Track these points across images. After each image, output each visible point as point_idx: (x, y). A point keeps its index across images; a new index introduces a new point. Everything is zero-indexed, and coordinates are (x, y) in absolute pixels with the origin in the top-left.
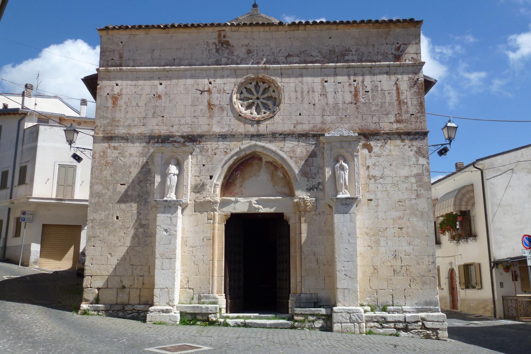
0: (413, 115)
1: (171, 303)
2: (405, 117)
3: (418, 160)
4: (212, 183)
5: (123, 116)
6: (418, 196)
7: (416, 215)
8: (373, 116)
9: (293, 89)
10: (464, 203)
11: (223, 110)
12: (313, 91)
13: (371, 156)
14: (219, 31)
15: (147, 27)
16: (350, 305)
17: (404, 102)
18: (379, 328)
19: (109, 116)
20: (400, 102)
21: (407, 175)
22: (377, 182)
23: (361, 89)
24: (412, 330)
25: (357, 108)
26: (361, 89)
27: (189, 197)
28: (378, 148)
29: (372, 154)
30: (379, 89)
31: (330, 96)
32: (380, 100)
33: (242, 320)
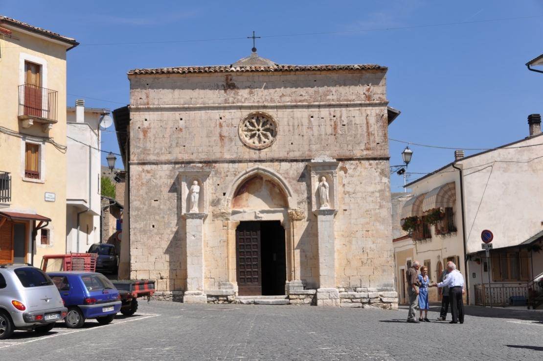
0: (379, 143)
1: (200, 289)
2: (373, 145)
3: (381, 179)
6: (381, 207)
9: (286, 123)
10: (445, 200)
11: (232, 141)
12: (302, 125)
13: (346, 176)
14: (227, 75)
16: (329, 287)
17: (372, 134)
18: (349, 303)
19: (141, 146)
21: (373, 191)
22: (351, 196)
23: (339, 123)
24: (373, 303)
25: (336, 138)
26: (339, 123)
28: (351, 170)
29: (347, 175)
30: (353, 123)
31: (315, 129)
32: (354, 132)
33: (253, 300)
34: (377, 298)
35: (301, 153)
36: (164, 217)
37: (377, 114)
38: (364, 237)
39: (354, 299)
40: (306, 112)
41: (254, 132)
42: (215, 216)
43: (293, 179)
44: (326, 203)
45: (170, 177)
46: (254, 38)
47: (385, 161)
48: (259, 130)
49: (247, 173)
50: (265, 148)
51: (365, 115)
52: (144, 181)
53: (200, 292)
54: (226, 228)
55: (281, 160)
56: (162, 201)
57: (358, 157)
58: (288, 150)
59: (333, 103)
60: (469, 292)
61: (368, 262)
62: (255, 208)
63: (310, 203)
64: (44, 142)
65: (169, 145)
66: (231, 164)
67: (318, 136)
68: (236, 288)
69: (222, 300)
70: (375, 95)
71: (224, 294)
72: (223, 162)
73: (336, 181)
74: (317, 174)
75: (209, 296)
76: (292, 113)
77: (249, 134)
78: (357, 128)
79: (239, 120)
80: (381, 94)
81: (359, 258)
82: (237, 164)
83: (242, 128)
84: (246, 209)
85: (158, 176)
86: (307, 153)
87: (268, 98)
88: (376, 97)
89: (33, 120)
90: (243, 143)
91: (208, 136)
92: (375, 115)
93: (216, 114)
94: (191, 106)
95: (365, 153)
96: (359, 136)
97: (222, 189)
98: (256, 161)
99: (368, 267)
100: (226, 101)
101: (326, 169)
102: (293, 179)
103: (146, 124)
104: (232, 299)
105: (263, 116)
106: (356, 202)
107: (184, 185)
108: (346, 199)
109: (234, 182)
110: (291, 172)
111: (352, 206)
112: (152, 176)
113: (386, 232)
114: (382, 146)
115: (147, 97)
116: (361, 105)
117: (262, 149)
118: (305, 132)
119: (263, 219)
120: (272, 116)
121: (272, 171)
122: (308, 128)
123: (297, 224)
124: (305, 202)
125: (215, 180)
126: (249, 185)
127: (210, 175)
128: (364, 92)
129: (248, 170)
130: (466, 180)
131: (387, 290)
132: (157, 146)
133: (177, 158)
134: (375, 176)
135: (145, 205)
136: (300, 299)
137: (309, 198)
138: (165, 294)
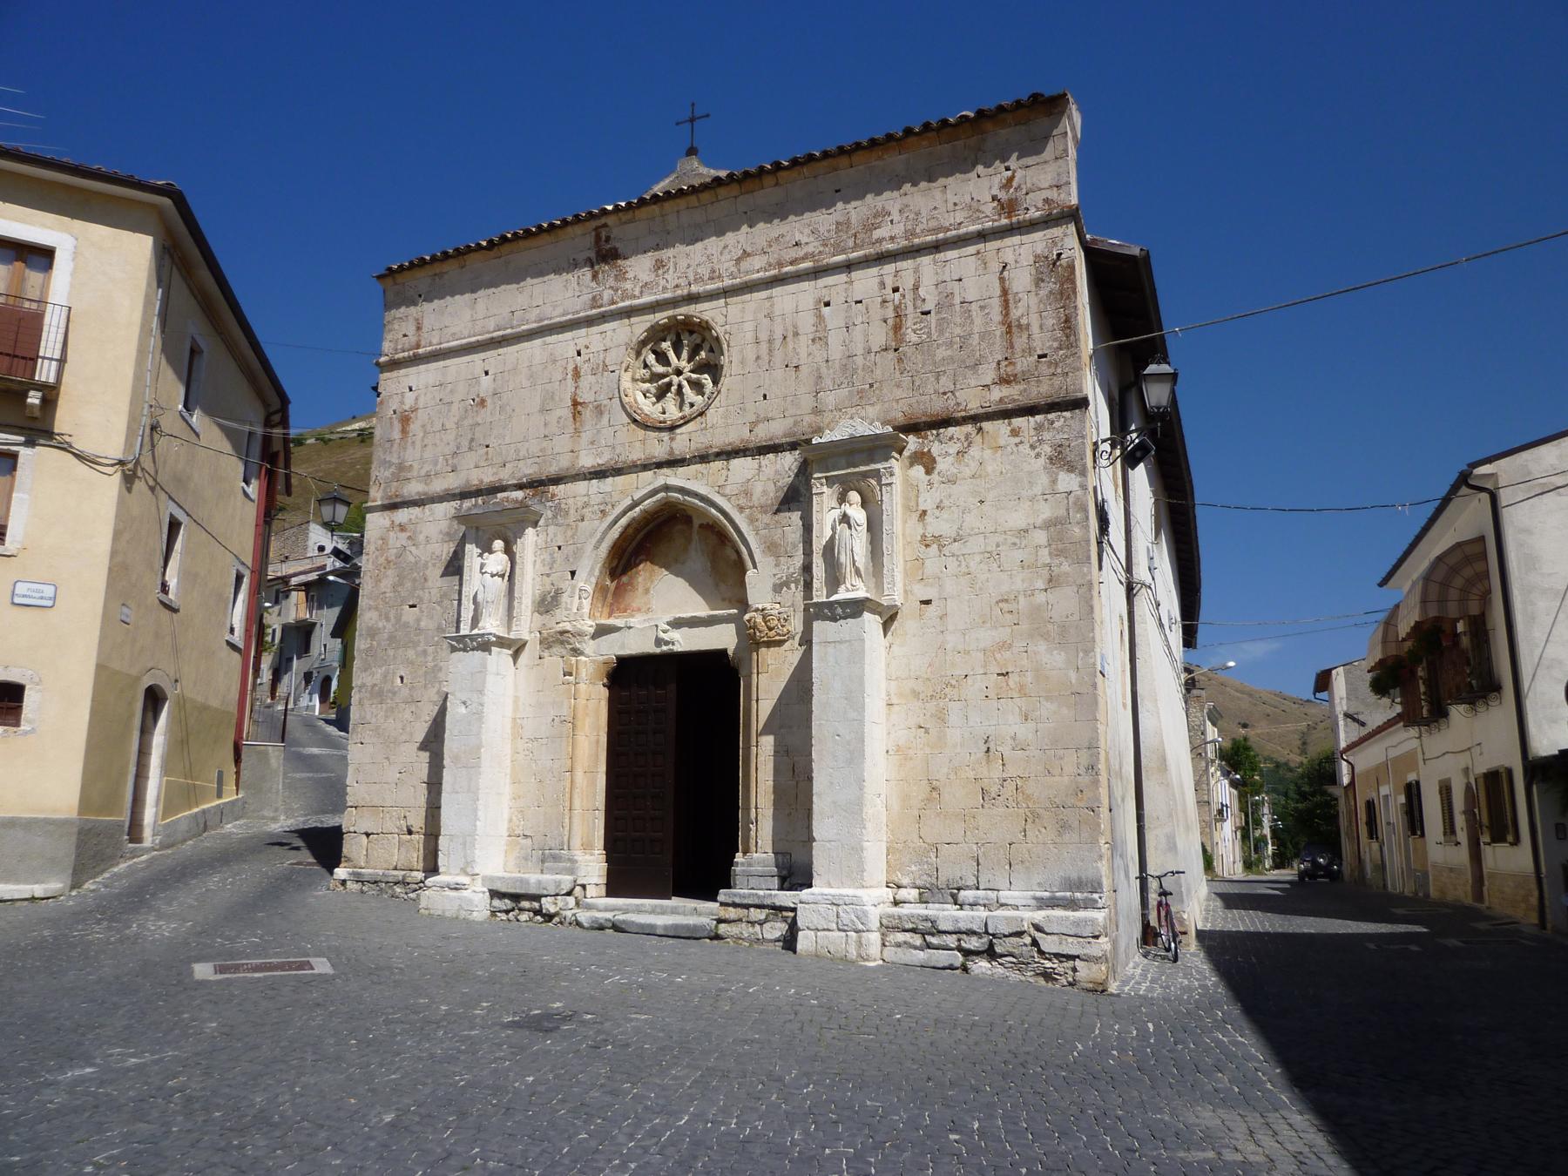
0: (1045, 356)
1: (469, 870)
2: (1023, 363)
3: (1054, 482)
4: (574, 587)
5: (418, 456)
6: (1053, 582)
7: (1046, 636)
8: (938, 376)
9: (750, 336)
10: (1454, 594)
11: (601, 413)
12: (796, 334)
13: (930, 484)
14: (596, 229)
15: (459, 253)
16: (843, 885)
17: (1020, 326)
18: (916, 948)
19: (395, 460)
20: (1010, 326)
21: (1024, 526)
22: (946, 551)
23: (910, 309)
24: (1002, 956)
25: (900, 360)
26: (910, 309)
27: (526, 627)
28: (950, 459)
29: (935, 477)
30: (957, 300)
31: (835, 339)
32: (958, 331)
33: (609, 915)
34: (1019, 934)
35: (790, 421)
36: (425, 652)
39: (933, 935)
40: (807, 291)
42: (547, 643)
43: (763, 509)
47: (1067, 414)
48: (679, 372)
51: (997, 267)
60: (1545, 887)
62: (668, 614)
63: (808, 586)
64: (30, 443)
65: (452, 448)
71: (533, 891)
73: (894, 501)
74: (830, 481)
75: (494, 894)
76: (768, 304)
77: (652, 387)
81: (971, 775)
86: (807, 419)
87: (704, 271)
89: (39, 394)
90: (629, 415)
91: (544, 410)
92: (1032, 259)
96: (975, 339)
98: (659, 465)
99: (1002, 810)
100: (595, 303)
101: (855, 463)
104: (552, 910)
108: (927, 562)
109: (599, 535)
110: (758, 489)
111: (950, 587)
113: (1073, 675)
114: (1057, 365)
116: (982, 236)
119: (677, 648)
123: (768, 656)
124: (796, 582)
125: (551, 535)
128: (995, 191)
130: (1511, 518)
131: (1072, 905)
132: (428, 454)
135: (388, 619)
136: (753, 923)
137: (807, 568)
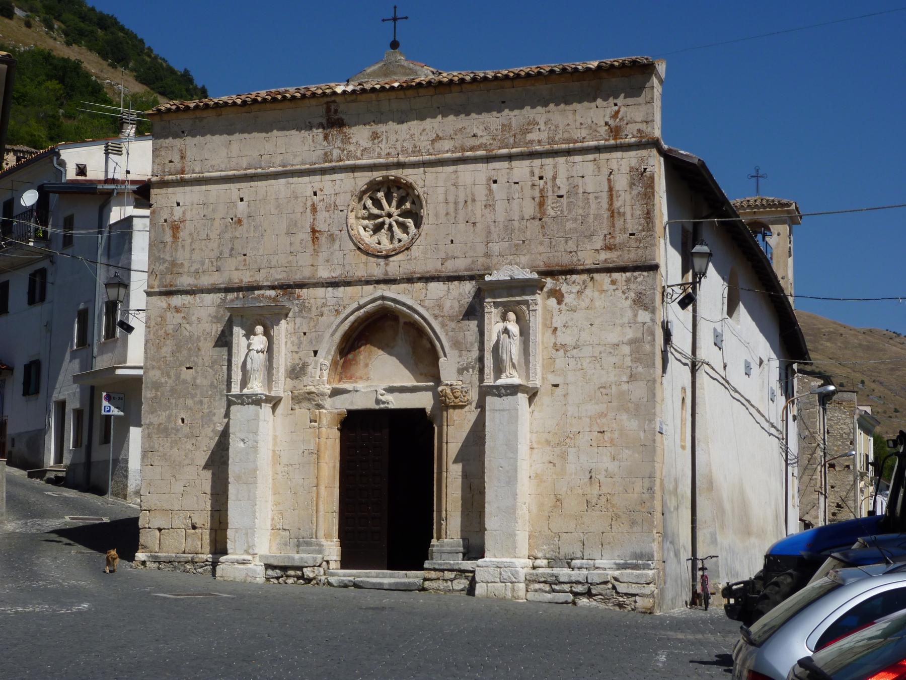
1: (251, 551)
2: (620, 238)
3: (636, 316)
9: (441, 198)
12: (474, 200)
13: (560, 311)
14: (327, 103)
16: (503, 556)
17: (619, 213)
18: (546, 592)
19: (168, 257)
22: (569, 354)
23: (550, 193)
25: (543, 227)
26: (550, 193)
29: (563, 306)
30: (581, 191)
31: (500, 206)
32: (580, 211)
33: (351, 579)
34: (606, 583)
35: (468, 261)
37: (631, 168)
38: (594, 444)
40: (482, 171)
41: (381, 220)
42: (297, 399)
43: (451, 318)
44: (509, 370)
45: (216, 319)
46: (395, 19)
47: (645, 274)
48: (390, 216)
49: (360, 308)
50: (397, 254)
52: (170, 329)
53: (250, 557)
54: (316, 424)
55: (427, 279)
56: (199, 369)
57: (587, 267)
58: (444, 256)
59: (538, 148)
61: (599, 502)
62: (382, 382)
66: (330, 289)
67: (506, 223)
68: (332, 550)
69: (293, 577)
70: (629, 125)
72: (316, 285)
73: (536, 321)
74: (496, 305)
75: (268, 567)
76: (454, 176)
78: (588, 202)
79: (349, 195)
80: (642, 122)
82: (341, 289)
83: (357, 213)
84: (360, 385)
85: (194, 318)
86: (481, 260)
87: (408, 145)
88: (632, 129)
91: (289, 233)
93: (305, 185)
94: (259, 171)
95: (603, 255)
97: (311, 342)
98: (378, 282)
100: (326, 157)
102: (451, 318)
103: (178, 212)
104: (311, 575)
105: (397, 184)
106: (579, 366)
107: (238, 332)
108: (557, 361)
109: (334, 327)
110: (447, 304)
112: (184, 318)
113: (642, 435)
115: (183, 157)
116: (598, 149)
117: (393, 256)
118: (478, 215)
119: (391, 406)
120: (414, 184)
121: (409, 302)
122: (485, 206)
124: (473, 368)
125: (298, 325)
126: (377, 328)
127: (290, 314)
128: (607, 119)
129: (362, 302)
132: (196, 256)
133: (230, 279)
134: (622, 309)
135: (169, 376)
136: (446, 580)
137: (481, 359)
138: (197, 560)
